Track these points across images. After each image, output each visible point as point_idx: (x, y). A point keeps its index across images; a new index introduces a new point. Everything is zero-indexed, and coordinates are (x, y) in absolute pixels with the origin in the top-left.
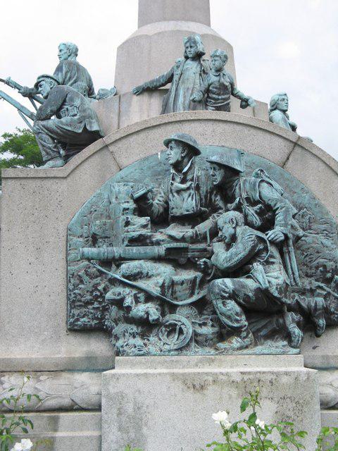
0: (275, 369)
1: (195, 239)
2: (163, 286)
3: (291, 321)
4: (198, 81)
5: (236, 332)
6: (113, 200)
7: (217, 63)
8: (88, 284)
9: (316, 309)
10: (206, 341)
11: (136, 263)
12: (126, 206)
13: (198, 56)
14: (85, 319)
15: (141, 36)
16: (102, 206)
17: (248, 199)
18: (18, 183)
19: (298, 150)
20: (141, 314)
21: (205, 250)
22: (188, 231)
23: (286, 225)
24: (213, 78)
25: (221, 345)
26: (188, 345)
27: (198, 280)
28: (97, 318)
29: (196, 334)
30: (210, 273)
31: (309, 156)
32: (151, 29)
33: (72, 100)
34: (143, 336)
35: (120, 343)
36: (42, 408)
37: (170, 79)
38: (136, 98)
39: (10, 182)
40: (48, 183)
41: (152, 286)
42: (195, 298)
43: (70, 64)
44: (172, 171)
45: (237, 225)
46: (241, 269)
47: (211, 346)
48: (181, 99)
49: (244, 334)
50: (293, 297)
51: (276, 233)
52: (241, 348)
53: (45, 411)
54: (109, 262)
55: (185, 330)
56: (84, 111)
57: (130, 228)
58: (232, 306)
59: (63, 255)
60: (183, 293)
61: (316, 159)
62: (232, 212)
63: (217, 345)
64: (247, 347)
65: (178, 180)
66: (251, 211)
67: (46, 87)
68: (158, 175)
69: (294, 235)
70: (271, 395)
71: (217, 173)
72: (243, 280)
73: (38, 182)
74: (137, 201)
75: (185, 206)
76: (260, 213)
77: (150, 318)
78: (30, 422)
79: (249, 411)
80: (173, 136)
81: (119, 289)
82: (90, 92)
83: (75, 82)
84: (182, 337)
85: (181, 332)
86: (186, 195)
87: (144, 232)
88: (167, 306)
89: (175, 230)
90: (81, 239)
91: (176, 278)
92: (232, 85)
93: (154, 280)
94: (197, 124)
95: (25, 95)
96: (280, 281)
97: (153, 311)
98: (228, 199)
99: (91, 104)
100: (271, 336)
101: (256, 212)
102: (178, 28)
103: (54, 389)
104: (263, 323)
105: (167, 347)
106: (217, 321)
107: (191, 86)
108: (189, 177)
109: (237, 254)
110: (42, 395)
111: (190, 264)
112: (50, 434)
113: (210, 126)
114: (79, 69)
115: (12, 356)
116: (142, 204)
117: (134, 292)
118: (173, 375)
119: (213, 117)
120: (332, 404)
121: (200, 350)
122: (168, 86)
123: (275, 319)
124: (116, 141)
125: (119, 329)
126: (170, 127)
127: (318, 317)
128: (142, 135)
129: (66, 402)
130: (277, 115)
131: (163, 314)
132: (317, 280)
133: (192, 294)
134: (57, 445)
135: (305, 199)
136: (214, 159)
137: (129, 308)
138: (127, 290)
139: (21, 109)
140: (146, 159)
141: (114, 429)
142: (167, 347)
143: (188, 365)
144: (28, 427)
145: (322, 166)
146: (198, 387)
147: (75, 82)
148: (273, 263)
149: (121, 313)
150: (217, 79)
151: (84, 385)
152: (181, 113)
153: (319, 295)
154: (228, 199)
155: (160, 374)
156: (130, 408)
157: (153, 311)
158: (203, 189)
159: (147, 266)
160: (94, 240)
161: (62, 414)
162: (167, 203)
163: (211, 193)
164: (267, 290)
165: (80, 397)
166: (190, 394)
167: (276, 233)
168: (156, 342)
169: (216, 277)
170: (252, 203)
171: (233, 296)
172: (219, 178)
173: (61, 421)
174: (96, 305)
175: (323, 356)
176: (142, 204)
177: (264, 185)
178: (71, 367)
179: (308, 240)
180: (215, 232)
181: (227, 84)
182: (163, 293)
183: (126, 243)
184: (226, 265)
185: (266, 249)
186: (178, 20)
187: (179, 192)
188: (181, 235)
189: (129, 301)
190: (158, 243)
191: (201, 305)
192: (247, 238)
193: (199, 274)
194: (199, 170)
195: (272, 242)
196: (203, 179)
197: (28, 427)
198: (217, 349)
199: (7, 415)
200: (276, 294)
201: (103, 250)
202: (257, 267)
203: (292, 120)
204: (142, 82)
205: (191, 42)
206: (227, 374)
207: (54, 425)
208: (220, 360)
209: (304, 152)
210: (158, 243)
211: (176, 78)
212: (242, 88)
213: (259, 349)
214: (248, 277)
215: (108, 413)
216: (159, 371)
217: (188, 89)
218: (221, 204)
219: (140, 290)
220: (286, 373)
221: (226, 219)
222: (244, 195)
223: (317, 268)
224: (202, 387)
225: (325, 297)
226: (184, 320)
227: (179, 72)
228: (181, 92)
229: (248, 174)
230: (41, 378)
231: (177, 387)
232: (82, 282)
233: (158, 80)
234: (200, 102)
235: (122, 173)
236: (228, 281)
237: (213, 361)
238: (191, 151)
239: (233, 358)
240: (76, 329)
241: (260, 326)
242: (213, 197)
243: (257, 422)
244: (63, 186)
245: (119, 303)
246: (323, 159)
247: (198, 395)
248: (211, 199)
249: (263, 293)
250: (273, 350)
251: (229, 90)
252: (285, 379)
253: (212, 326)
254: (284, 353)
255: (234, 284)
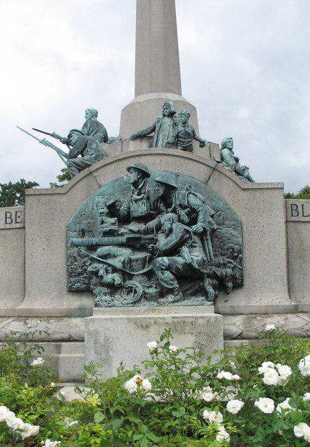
0: (195, 315)
1: (147, 232)
2: (124, 263)
3: (208, 285)
4: (171, 130)
5: (171, 291)
6: (95, 207)
7: (183, 119)
8: (80, 262)
9: (226, 276)
10: (152, 297)
11: (107, 248)
12: (102, 211)
13: (171, 115)
14: (78, 284)
15: (136, 103)
16: (88, 213)
17: (180, 205)
18: (35, 198)
19: (216, 173)
20: (109, 280)
21: (152, 239)
22: (142, 227)
23: (204, 222)
24: (180, 128)
25: (161, 300)
26: (139, 300)
27: (147, 258)
28: (85, 284)
29: (144, 293)
30: (154, 253)
31: (222, 176)
32: (142, 98)
33: (90, 144)
34: (111, 294)
35: (97, 299)
36: (51, 339)
37: (153, 130)
38: (132, 142)
39: (30, 197)
40: (54, 198)
41: (117, 263)
42: (145, 270)
43: (92, 122)
44: (132, 188)
45: (173, 222)
46: (174, 251)
47: (155, 301)
48: (160, 142)
49: (176, 293)
50: (211, 269)
51: (198, 227)
52: (173, 302)
53: (53, 341)
54: (92, 248)
55: (138, 290)
56: (99, 152)
57: (105, 225)
58: (168, 274)
59: (64, 244)
60: (137, 267)
61: (227, 179)
62: (170, 214)
63: (159, 300)
64: (178, 301)
65: (136, 193)
66: (183, 213)
67: (75, 138)
68: (124, 191)
69: (211, 228)
70: (192, 331)
71: (160, 189)
72: (176, 258)
73: (48, 197)
74: (109, 207)
75: (140, 210)
76: (188, 214)
77: (116, 283)
78: (42, 347)
79: (165, 341)
80: (132, 165)
81: (96, 265)
82: (105, 139)
83: (95, 133)
84: (136, 295)
85: (135, 292)
86: (140, 203)
87: (113, 227)
88: (127, 276)
89: (134, 226)
90: (75, 233)
91: (133, 257)
92: (193, 132)
93: (118, 258)
94: (150, 157)
95: (64, 143)
96: (199, 258)
97: (117, 278)
98: (168, 205)
99: (104, 147)
100: (195, 294)
101: (186, 214)
102: (160, 97)
103: (58, 328)
104: (190, 285)
105: (126, 301)
106: (158, 285)
107: (167, 134)
108: (143, 191)
109: (171, 241)
110: (50, 331)
111: (143, 248)
112: (56, 355)
113: (158, 158)
114: (98, 125)
115: (33, 307)
116: (112, 210)
117: (105, 266)
118: (129, 320)
119: (182, 155)
120: (235, 336)
121: (147, 303)
122: (152, 134)
123: (197, 283)
124: (97, 169)
125: (98, 290)
126: (132, 160)
127: (228, 281)
128: (114, 165)
129: (66, 336)
130: (226, 152)
131: (124, 281)
132: (228, 258)
133: (144, 268)
134: (59, 361)
135: (221, 205)
136: (158, 179)
137: (102, 277)
138: (101, 265)
139: (59, 152)
140: (117, 180)
141: (93, 352)
142: (126, 301)
143: (139, 313)
144: (41, 350)
145: (232, 184)
146: (144, 326)
147: (95, 133)
148: (195, 246)
149: (98, 280)
150: (183, 128)
151: (76, 325)
152: (160, 150)
153: (229, 267)
154: (168, 205)
155: (106, 319)
156: (102, 339)
157: (117, 278)
158: (152, 199)
159: (114, 249)
160: (83, 233)
161: (63, 343)
162: (129, 208)
163: (157, 202)
164: (190, 264)
165: (74, 333)
166: (139, 331)
167: (198, 227)
168: (119, 298)
169: (159, 256)
170: (181, 206)
171: (169, 268)
172: (161, 191)
173: (63, 348)
174: (85, 275)
175: (231, 307)
176: (112, 210)
177: (191, 196)
178: (70, 314)
179: (223, 231)
180: (159, 227)
181: (190, 132)
182: (124, 267)
183: (102, 235)
184: (164, 248)
185: (190, 238)
186: (160, 92)
187: (136, 201)
188: (138, 229)
189: (101, 272)
190: (122, 235)
191: (150, 275)
192: (179, 228)
193: (148, 255)
194: (150, 187)
195: (195, 233)
196: (152, 192)
197: (41, 350)
198: (158, 303)
199: (28, 343)
200: (196, 267)
201: (87, 239)
202: (185, 249)
203: (236, 155)
204: (136, 131)
205: (167, 106)
206: (163, 318)
207: (58, 349)
208: (159, 309)
209: (220, 174)
210: (122, 235)
211: (157, 129)
212: (203, 134)
213: (185, 302)
214: (179, 256)
215: (89, 342)
216: (120, 316)
217: (165, 135)
218: (164, 209)
219: (109, 265)
220: (202, 317)
221: (166, 218)
222: (178, 203)
223: (228, 249)
224: (147, 327)
225: (233, 269)
226: (137, 284)
227: (159, 125)
228: (161, 138)
229: (182, 189)
230: (51, 321)
231: (131, 327)
232: (76, 260)
233: (146, 130)
234: (173, 144)
235: (102, 190)
236: (165, 259)
237: (155, 310)
238: (144, 174)
239: (168, 308)
240: (73, 291)
241: (187, 287)
242: (158, 204)
243: (171, 347)
244: (64, 199)
245: (96, 273)
246: (141, 153)
247: (144, 332)
248: (157, 206)
249: (188, 266)
250: (195, 303)
251: (192, 135)
252: (201, 321)
253: (156, 288)
254: (202, 305)
255: (169, 260)
